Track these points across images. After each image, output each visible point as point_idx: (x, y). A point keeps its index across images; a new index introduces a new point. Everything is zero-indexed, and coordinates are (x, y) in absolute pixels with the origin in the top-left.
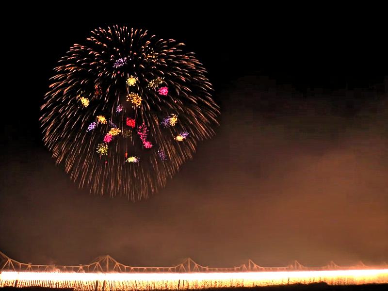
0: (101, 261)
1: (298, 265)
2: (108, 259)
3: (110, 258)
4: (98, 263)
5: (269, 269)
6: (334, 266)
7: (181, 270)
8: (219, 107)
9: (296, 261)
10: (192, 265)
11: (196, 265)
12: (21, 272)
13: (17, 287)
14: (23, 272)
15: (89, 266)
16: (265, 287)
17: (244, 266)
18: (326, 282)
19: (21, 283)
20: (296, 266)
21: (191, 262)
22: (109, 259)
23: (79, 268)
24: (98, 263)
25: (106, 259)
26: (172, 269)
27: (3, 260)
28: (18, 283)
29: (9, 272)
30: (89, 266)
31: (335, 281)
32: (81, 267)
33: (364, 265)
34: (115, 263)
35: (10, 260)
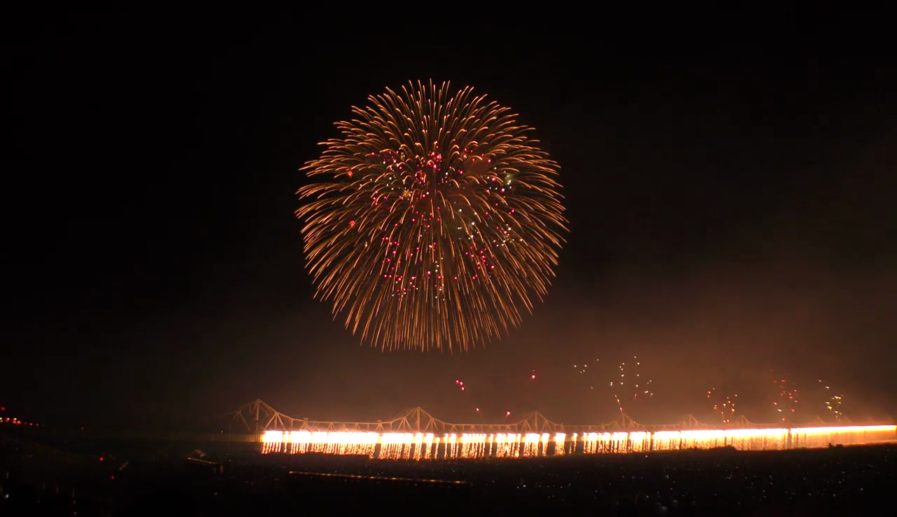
0: (409, 416)
1: (692, 420)
2: (418, 412)
3: (422, 410)
4: (405, 419)
5: (488, 428)
6: (745, 422)
7: (524, 428)
8: (495, 102)
9: (743, 416)
10: (541, 422)
11: (546, 421)
12: (295, 432)
13: (312, 450)
14: (670, 432)
15: (391, 423)
16: (706, 450)
17: (526, 422)
18: (735, 445)
19: (267, 448)
20: (624, 425)
21: (538, 416)
22: (420, 412)
23: (377, 425)
24: (405, 419)
25: (416, 413)
26: (493, 427)
27: (267, 415)
28: (463, 450)
29: (393, 434)
30: (391, 423)
31: (705, 443)
32: (603, 427)
33: (822, 422)
34: (429, 419)
35: (277, 414)
